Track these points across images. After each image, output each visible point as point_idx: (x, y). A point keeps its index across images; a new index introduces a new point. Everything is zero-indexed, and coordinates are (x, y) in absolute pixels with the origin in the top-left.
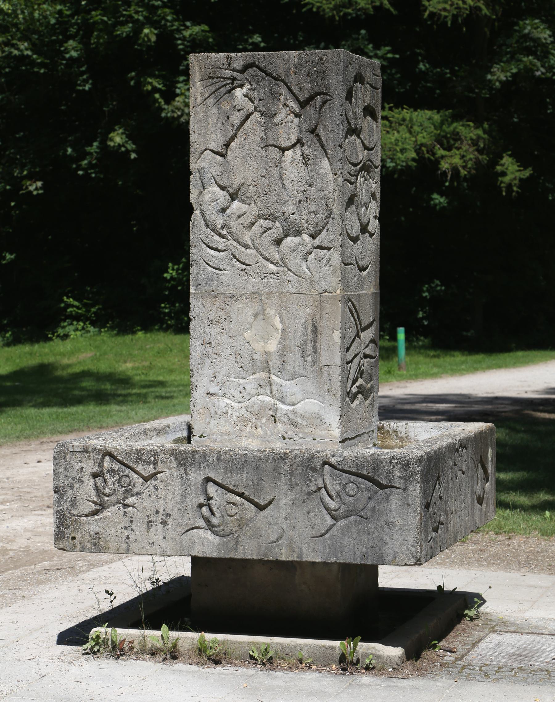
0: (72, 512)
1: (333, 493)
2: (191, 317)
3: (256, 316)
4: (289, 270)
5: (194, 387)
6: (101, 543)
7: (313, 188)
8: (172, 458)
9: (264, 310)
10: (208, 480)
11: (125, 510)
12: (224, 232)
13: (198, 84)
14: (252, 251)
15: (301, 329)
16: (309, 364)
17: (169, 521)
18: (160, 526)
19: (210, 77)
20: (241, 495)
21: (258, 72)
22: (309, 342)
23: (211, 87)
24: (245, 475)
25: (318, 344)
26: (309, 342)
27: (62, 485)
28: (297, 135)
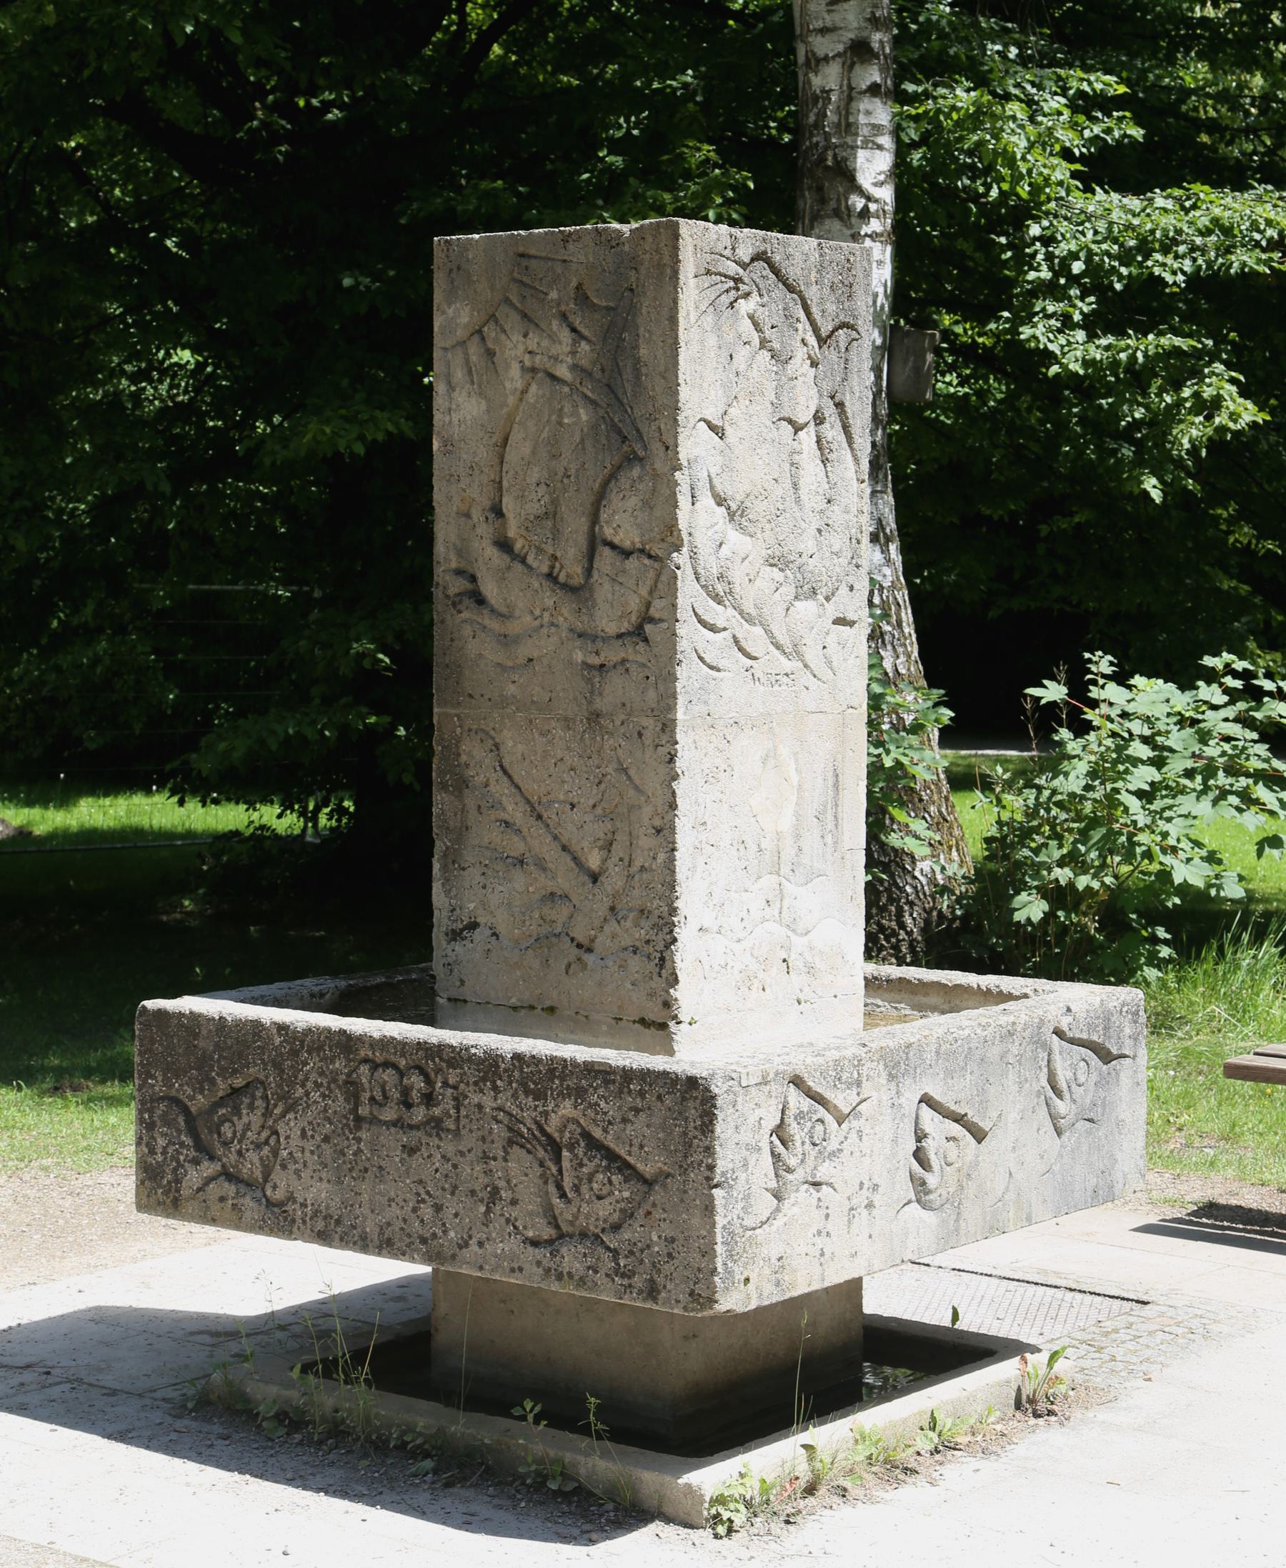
0: (747, 1223)
1: (1063, 1085)
2: (679, 772)
3: (764, 761)
4: (806, 666)
5: (683, 920)
6: (786, 1278)
7: (836, 508)
8: (881, 1067)
9: (775, 748)
10: (926, 1100)
11: (820, 1195)
12: (720, 588)
13: (692, 282)
14: (758, 630)
15: (820, 780)
16: (829, 850)
17: (877, 1199)
18: (865, 1212)
19: (708, 272)
20: (959, 1119)
21: (767, 272)
22: (829, 806)
23: (707, 292)
24: (968, 1077)
25: (840, 809)
26: (829, 806)
27: (731, 1166)
28: (816, 401)
